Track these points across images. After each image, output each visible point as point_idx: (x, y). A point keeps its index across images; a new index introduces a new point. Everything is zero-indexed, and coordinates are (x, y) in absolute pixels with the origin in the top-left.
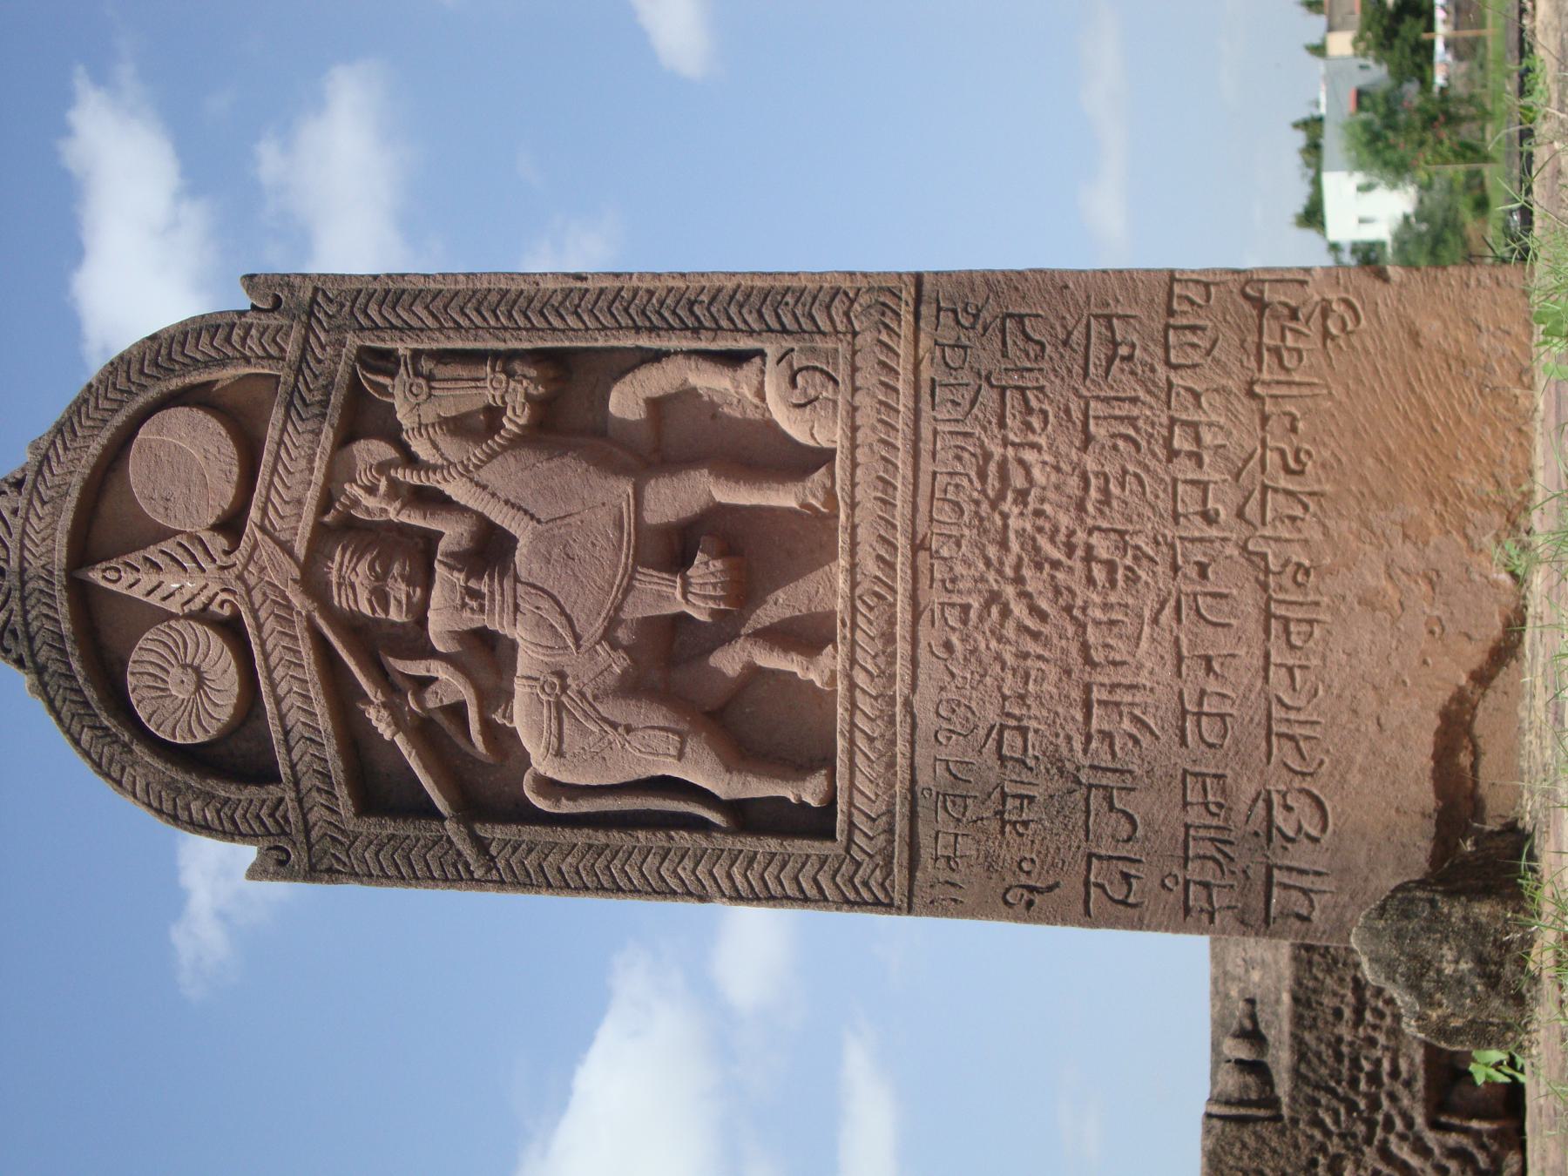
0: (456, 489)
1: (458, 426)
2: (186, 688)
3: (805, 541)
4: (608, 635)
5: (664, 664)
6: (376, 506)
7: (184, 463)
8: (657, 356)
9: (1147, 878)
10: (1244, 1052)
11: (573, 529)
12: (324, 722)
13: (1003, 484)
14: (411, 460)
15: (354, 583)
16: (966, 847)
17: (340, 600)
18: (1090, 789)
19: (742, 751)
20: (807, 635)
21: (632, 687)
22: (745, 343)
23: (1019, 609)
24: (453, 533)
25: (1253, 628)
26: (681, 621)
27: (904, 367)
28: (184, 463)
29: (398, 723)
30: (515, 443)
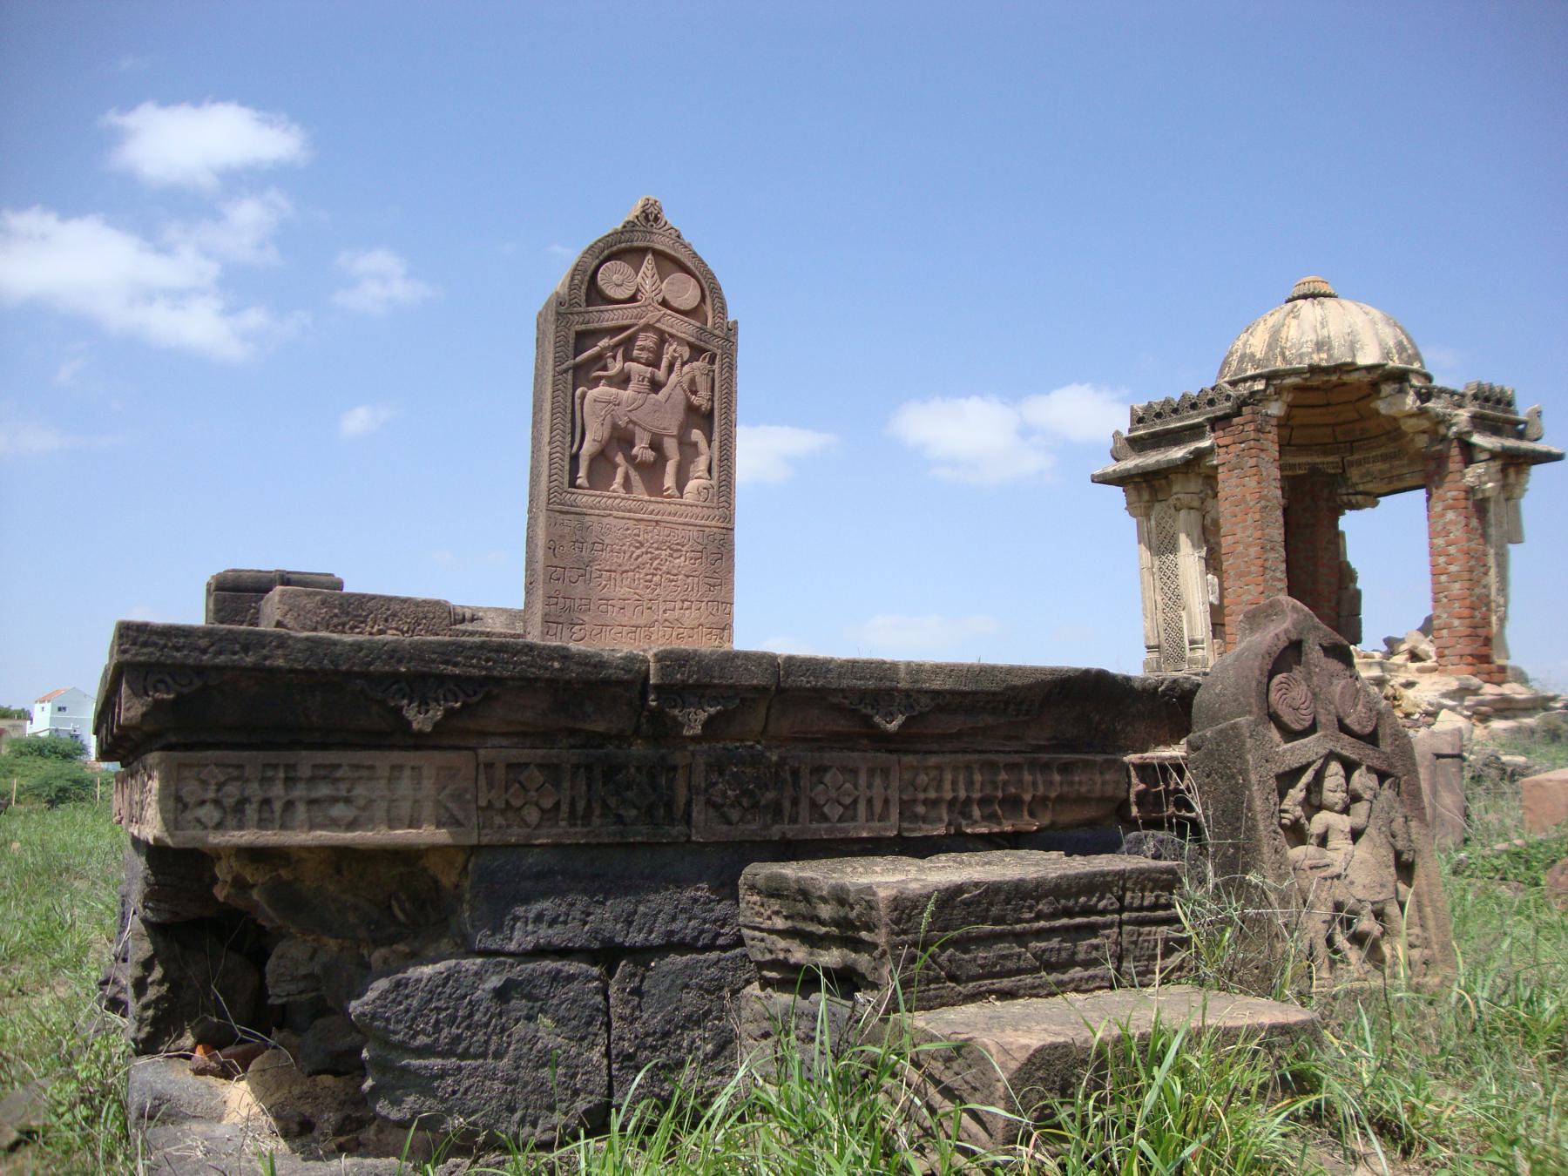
0: (674, 378)
1: (693, 381)
2: (615, 279)
3: (655, 488)
4: (631, 421)
5: (621, 439)
6: (670, 350)
7: (686, 293)
8: (709, 442)
9: (559, 585)
10: (468, 615)
11: (661, 414)
12: (605, 324)
13: (675, 550)
14: (683, 364)
15: (646, 341)
16: (567, 530)
17: (642, 336)
18: (584, 568)
19: (595, 459)
20: (627, 484)
21: (615, 427)
22: (715, 473)
23: (638, 552)
24: (661, 374)
25: (633, 623)
26: (633, 446)
27: (708, 523)
28: (686, 293)
29: (604, 349)
30: (688, 399)
